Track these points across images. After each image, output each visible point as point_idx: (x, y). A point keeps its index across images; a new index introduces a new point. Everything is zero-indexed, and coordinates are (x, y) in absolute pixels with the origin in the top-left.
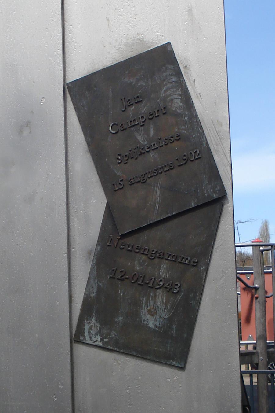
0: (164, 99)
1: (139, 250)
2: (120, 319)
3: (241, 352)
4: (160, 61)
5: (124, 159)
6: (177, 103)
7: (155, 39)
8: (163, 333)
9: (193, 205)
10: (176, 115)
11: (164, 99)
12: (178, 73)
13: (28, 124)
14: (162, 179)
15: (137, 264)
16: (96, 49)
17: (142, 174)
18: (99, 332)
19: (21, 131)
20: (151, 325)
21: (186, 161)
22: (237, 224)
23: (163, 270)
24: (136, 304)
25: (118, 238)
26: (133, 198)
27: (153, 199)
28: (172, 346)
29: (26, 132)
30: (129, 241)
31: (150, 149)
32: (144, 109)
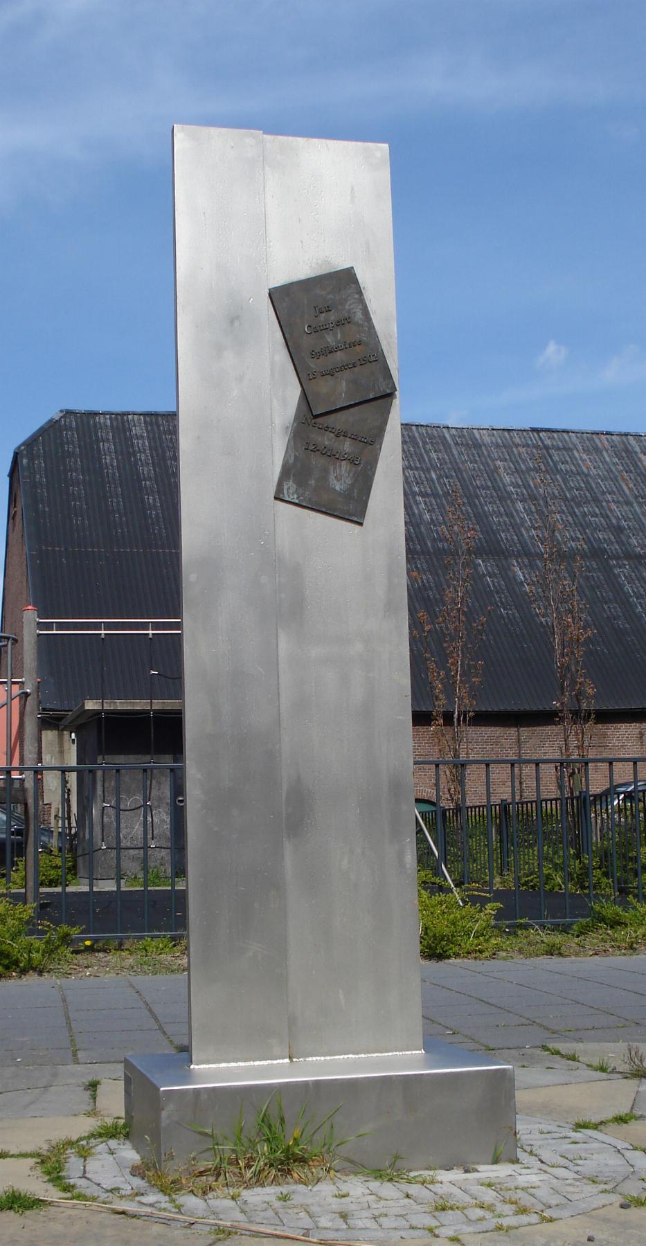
0: (349, 311)
1: (327, 429)
2: (312, 482)
3: (167, 761)
4: (345, 280)
5: (315, 355)
6: (359, 315)
7: (342, 264)
8: (347, 495)
9: (371, 396)
10: (358, 324)
11: (349, 311)
12: (360, 293)
13: (238, 317)
14: (347, 374)
15: (326, 440)
16: (295, 262)
17: (591, 1234)
18: (296, 492)
19: (232, 322)
20: (337, 488)
21: (365, 361)
22: (250, 1222)
23: (347, 446)
24: (325, 471)
25: (311, 416)
26: (323, 386)
27: (339, 390)
28: (351, 508)
29: (236, 324)
30: (319, 420)
31: (338, 349)
32: (333, 317)
